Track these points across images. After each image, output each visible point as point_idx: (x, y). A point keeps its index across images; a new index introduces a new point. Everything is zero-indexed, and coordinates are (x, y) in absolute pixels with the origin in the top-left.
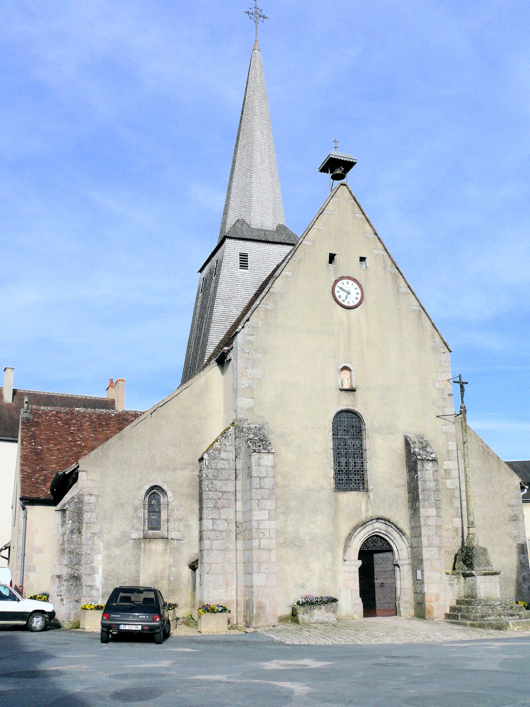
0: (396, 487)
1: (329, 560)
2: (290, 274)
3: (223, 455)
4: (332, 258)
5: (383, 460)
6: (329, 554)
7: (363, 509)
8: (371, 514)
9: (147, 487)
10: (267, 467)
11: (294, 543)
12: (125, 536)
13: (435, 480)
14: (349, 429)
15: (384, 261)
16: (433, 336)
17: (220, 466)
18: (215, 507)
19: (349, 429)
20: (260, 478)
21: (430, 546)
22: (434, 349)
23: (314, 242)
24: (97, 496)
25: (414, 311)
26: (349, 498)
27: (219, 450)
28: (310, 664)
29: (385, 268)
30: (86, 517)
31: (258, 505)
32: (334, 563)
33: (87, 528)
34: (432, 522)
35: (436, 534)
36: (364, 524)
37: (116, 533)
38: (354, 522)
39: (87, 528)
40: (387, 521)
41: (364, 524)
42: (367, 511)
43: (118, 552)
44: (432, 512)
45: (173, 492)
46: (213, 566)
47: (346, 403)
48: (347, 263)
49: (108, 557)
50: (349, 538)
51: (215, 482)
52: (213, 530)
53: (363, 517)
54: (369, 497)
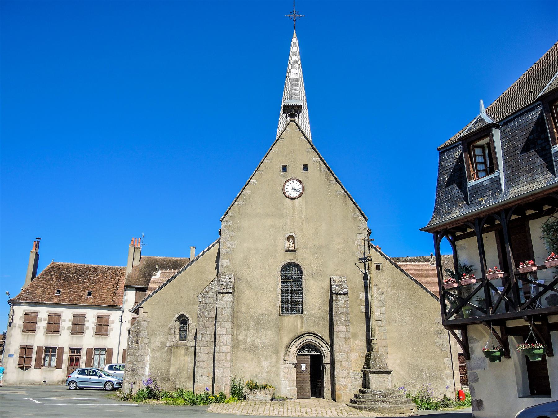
0: (323, 311)
1: (274, 360)
2: (255, 181)
3: (210, 295)
4: (284, 168)
5: (314, 296)
6: (274, 356)
7: (299, 327)
8: (305, 330)
9: (177, 315)
10: (227, 301)
11: (254, 349)
12: (163, 345)
13: (345, 307)
14: (292, 275)
15: (320, 165)
16: (354, 211)
17: (208, 301)
18: (203, 327)
19: (292, 275)
20: (222, 308)
21: (340, 352)
22: (354, 218)
23: (271, 159)
24: (148, 322)
25: (341, 195)
26: (290, 320)
27: (208, 292)
28: (117, 404)
29: (321, 171)
30: (142, 334)
31: (220, 325)
32: (277, 362)
33: (142, 340)
34: (342, 335)
35: (345, 344)
36: (299, 337)
37: (158, 343)
38: (292, 335)
39: (142, 340)
40: (315, 335)
41: (299, 337)
42: (302, 327)
43: (159, 354)
44: (343, 328)
45: (192, 318)
46: (201, 363)
47: (290, 258)
48: (295, 170)
49: (153, 357)
50: (288, 346)
51: (204, 311)
52: (202, 341)
53: (299, 332)
54: (303, 318)
